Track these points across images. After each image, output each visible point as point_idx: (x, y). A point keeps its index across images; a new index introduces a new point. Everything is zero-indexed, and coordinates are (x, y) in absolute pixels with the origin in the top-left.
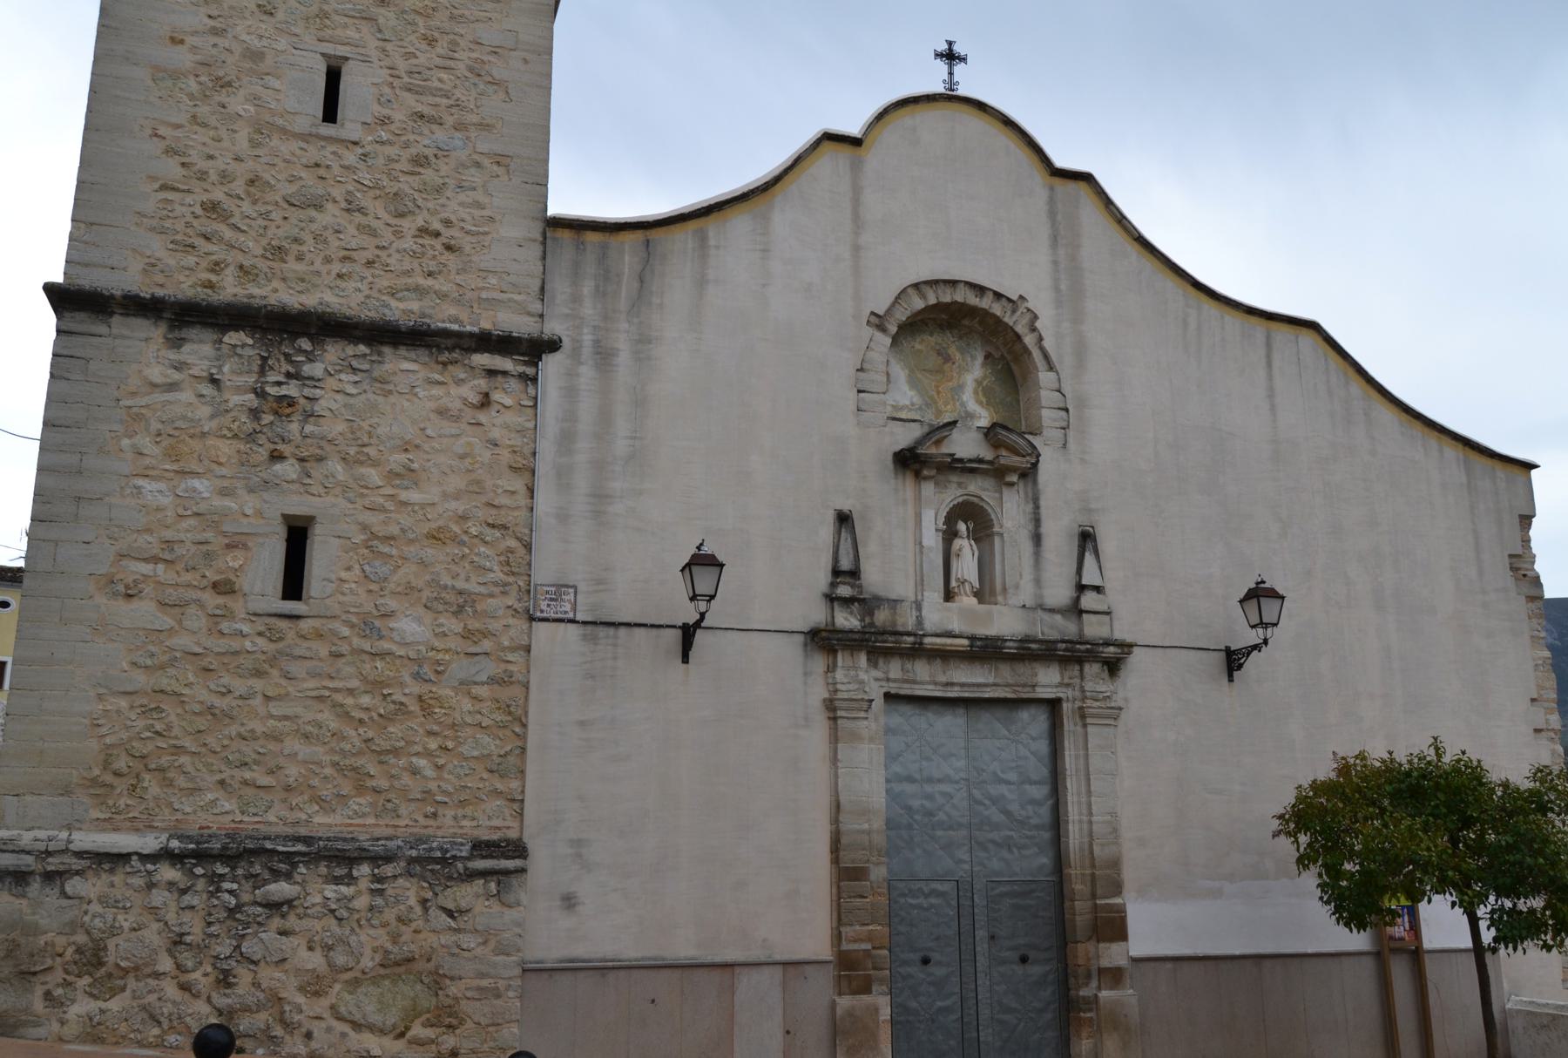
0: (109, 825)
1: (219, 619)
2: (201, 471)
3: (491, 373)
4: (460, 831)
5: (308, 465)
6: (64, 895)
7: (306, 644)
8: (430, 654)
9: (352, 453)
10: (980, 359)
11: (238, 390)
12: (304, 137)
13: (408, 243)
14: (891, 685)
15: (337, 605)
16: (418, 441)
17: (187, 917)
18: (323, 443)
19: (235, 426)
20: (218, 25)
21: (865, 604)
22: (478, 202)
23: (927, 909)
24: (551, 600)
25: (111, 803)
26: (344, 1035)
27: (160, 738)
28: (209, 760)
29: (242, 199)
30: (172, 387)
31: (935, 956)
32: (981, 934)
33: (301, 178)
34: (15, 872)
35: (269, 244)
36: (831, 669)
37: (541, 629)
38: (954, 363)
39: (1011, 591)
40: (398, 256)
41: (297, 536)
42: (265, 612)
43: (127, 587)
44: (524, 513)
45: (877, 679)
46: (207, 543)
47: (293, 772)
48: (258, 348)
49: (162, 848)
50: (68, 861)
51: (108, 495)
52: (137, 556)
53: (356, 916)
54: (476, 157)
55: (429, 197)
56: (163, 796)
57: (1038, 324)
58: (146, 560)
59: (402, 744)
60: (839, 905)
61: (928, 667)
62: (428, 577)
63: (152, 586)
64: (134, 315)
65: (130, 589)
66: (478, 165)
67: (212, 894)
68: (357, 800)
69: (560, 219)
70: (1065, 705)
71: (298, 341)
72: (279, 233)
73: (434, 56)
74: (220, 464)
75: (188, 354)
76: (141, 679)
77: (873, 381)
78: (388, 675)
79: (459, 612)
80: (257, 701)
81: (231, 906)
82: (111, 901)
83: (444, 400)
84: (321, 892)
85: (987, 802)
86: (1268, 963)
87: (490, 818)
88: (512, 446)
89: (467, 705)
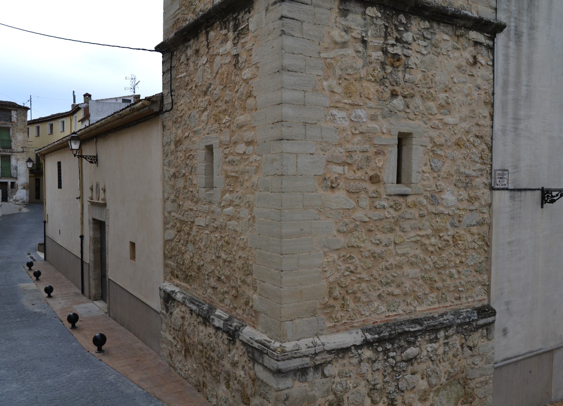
0: (335, 329)
1: (374, 200)
2: (361, 104)
5: (407, 100)
7: (410, 211)
11: (375, 49)
15: (422, 187)
16: (450, 86)
18: (414, 86)
24: (501, 178)
25: (334, 316)
28: (374, 284)
30: (344, 45)
34: (302, 368)
37: (496, 193)
42: (394, 193)
44: (488, 129)
48: (383, 20)
49: (364, 340)
50: (325, 357)
51: (319, 121)
52: (336, 161)
53: (439, 358)
56: (356, 308)
58: (339, 164)
62: (455, 168)
67: (386, 360)
75: (352, 21)
76: (342, 240)
78: (442, 225)
80: (392, 247)
82: (344, 374)
83: (460, 60)
89: (469, 238)
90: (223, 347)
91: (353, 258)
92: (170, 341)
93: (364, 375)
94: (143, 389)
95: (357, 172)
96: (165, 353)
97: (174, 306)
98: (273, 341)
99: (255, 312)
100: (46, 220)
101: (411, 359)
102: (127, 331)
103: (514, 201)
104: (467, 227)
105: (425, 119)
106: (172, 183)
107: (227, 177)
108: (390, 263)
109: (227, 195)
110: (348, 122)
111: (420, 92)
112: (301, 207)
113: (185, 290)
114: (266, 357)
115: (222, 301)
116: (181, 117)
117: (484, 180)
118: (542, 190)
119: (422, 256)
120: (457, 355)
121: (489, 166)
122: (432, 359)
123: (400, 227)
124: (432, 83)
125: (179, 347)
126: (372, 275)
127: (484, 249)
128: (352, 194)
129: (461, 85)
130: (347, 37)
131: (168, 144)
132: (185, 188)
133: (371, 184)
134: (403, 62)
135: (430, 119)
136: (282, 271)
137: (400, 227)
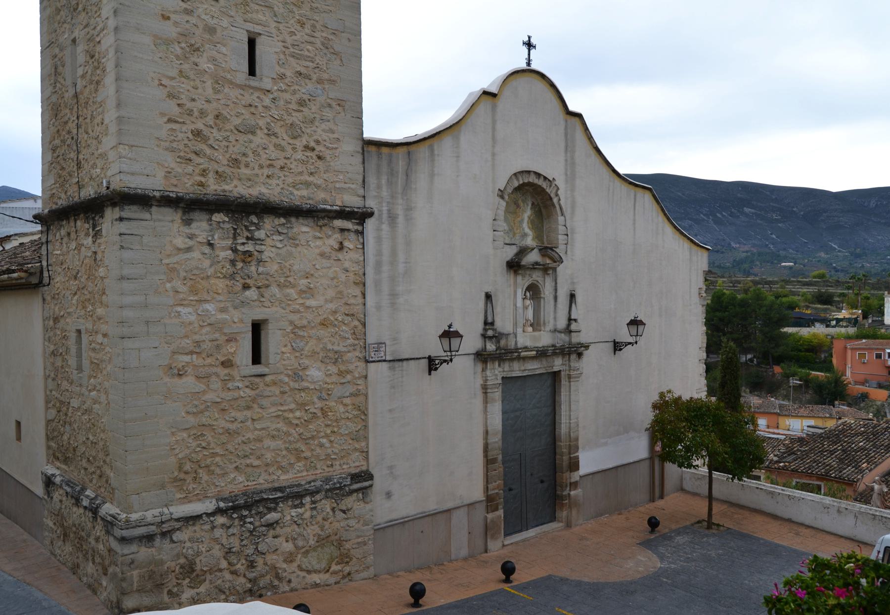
0: (186, 500)
2: (209, 299)
3: (342, 230)
4: (342, 471)
5: (261, 290)
6: (173, 541)
7: (269, 389)
8: (325, 386)
9: (282, 281)
11: (223, 249)
12: (242, 87)
13: (299, 155)
14: (505, 373)
15: (282, 366)
16: (312, 272)
17: (232, 540)
18: (268, 277)
19: (224, 271)
20: (189, 7)
21: (498, 337)
22: (331, 129)
24: (376, 351)
25: (185, 488)
26: (304, 577)
27: (205, 450)
28: (230, 457)
29: (213, 128)
30: (189, 249)
33: (242, 114)
34: (147, 536)
35: (230, 157)
39: (547, 324)
40: (295, 163)
41: (257, 328)
42: (249, 375)
43: (179, 370)
44: (361, 307)
46: (217, 340)
47: (269, 456)
48: (231, 223)
49: (216, 508)
50: (173, 524)
51: (163, 318)
52: (182, 352)
53: (305, 522)
54: (328, 101)
55: (308, 126)
57: (559, 192)
58: (186, 354)
59: (316, 433)
60: (487, 475)
62: (321, 346)
63: (191, 367)
64: (164, 206)
65: (180, 371)
66: (330, 106)
67: (242, 526)
68: (299, 464)
69: (372, 141)
70: (562, 373)
71: (250, 217)
72: (235, 150)
73: (304, 34)
74: (218, 294)
75: (196, 229)
76: (192, 420)
77: (499, 225)
78: (308, 400)
79: (335, 362)
80: (249, 423)
81: (251, 530)
83: (323, 248)
84: (290, 514)
86: (619, 469)
87: (354, 462)
88: (355, 271)
89: (342, 409)
90: (90, 525)
91: (205, 435)
92: (51, 528)
94: (14, 577)
96: (47, 542)
97: (54, 490)
98: (122, 513)
99: (113, 489)
101: (273, 524)
102: (14, 523)
104: (339, 398)
105: (283, 305)
106: (51, 360)
107: (92, 363)
108: (247, 437)
109: (92, 380)
110: (195, 316)
111: (276, 281)
112: (145, 394)
113: (64, 473)
114: (115, 528)
115: (91, 481)
116: (58, 294)
117: (357, 354)
118: (429, 358)
120: (328, 519)
121: (363, 341)
122: (297, 522)
123: (259, 404)
124: (290, 272)
125: (58, 532)
128: (201, 379)
129: (324, 270)
130: (191, 243)
131: (48, 318)
132: (62, 367)
133: (223, 369)
135: (289, 305)
136: (126, 451)
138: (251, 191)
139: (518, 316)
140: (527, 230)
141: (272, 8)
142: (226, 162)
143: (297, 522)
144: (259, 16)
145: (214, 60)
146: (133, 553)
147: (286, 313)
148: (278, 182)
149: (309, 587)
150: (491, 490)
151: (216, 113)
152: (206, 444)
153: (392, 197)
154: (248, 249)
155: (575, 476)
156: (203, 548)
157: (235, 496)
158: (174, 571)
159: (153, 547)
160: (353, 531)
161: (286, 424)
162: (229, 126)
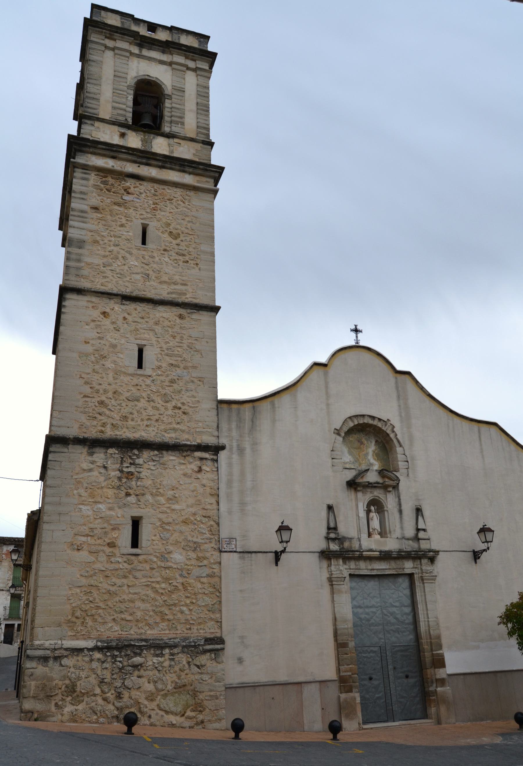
0: (75, 637)
3: (201, 459)
6: (61, 665)
7: (141, 565)
9: (154, 492)
10: (374, 443)
11: (114, 470)
12: (132, 375)
13: (170, 412)
14: (352, 571)
16: (177, 486)
17: (105, 672)
18: (144, 489)
19: (113, 484)
21: (341, 540)
23: (370, 658)
24: (228, 544)
25: (75, 629)
26: (162, 716)
28: (109, 611)
30: (91, 470)
31: (374, 676)
32: (390, 667)
33: (131, 390)
34: (44, 657)
35: (122, 415)
36: (329, 566)
37: (224, 555)
38: (364, 445)
39: (392, 532)
41: (136, 523)
43: (78, 546)
44: (216, 511)
45: (346, 569)
47: (139, 614)
49: (95, 646)
50: (62, 652)
51: (70, 512)
53: (165, 669)
54: (192, 379)
55: (176, 394)
56: (93, 625)
57: (395, 430)
58: (83, 536)
59: (177, 602)
60: (338, 658)
61: (364, 563)
62: (183, 538)
66: (193, 382)
67: (113, 663)
68: (162, 624)
70: (415, 576)
71: (133, 451)
72: (125, 411)
73: (175, 342)
74: (108, 498)
76: (84, 581)
77: (337, 455)
79: (195, 550)
80: (125, 588)
83: (186, 470)
85: (389, 615)
89: (199, 586)
93: (95, 670)
95: (97, 540)
100: (24, 640)
101: (138, 666)
103: (244, 560)
105: (154, 508)
108: (123, 598)
110: (92, 512)
111: (150, 492)
112: (54, 560)
119: (153, 595)
120: (184, 670)
123: (133, 575)
124: (160, 485)
126: (107, 605)
127: (216, 595)
128: (92, 553)
129: (187, 485)
130: (92, 466)
133: (109, 548)
134: (135, 476)
135: (159, 507)
137: (133, 575)
138: (134, 435)
139: (360, 524)
140: (372, 461)
141: (153, 330)
142: (119, 418)
143: (158, 668)
144: (145, 335)
145: (115, 361)
146: (33, 668)
147: (156, 513)
148: (154, 429)
149: (166, 726)
150: (343, 672)
151: (114, 390)
152: (93, 599)
153: (241, 436)
154: (131, 470)
155: (441, 673)
156: (83, 675)
157: (111, 640)
158: (60, 689)
159: (47, 666)
160: (206, 685)
161: (154, 592)
162: (122, 398)
